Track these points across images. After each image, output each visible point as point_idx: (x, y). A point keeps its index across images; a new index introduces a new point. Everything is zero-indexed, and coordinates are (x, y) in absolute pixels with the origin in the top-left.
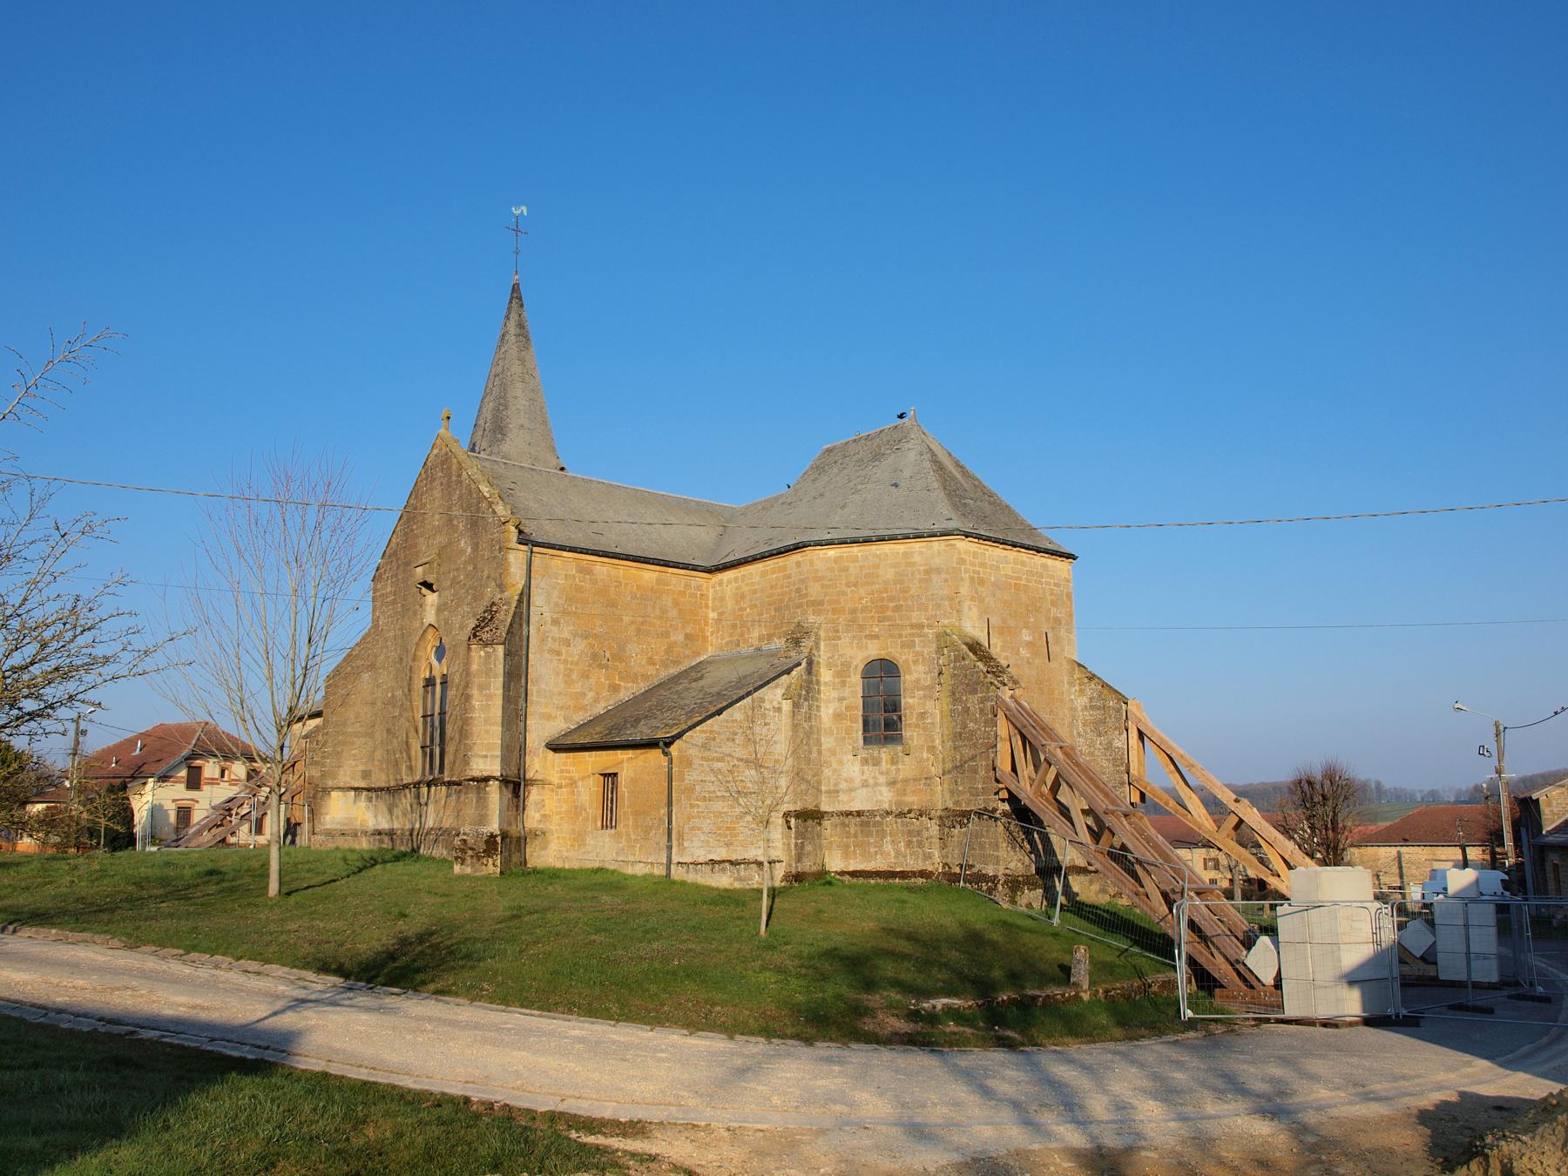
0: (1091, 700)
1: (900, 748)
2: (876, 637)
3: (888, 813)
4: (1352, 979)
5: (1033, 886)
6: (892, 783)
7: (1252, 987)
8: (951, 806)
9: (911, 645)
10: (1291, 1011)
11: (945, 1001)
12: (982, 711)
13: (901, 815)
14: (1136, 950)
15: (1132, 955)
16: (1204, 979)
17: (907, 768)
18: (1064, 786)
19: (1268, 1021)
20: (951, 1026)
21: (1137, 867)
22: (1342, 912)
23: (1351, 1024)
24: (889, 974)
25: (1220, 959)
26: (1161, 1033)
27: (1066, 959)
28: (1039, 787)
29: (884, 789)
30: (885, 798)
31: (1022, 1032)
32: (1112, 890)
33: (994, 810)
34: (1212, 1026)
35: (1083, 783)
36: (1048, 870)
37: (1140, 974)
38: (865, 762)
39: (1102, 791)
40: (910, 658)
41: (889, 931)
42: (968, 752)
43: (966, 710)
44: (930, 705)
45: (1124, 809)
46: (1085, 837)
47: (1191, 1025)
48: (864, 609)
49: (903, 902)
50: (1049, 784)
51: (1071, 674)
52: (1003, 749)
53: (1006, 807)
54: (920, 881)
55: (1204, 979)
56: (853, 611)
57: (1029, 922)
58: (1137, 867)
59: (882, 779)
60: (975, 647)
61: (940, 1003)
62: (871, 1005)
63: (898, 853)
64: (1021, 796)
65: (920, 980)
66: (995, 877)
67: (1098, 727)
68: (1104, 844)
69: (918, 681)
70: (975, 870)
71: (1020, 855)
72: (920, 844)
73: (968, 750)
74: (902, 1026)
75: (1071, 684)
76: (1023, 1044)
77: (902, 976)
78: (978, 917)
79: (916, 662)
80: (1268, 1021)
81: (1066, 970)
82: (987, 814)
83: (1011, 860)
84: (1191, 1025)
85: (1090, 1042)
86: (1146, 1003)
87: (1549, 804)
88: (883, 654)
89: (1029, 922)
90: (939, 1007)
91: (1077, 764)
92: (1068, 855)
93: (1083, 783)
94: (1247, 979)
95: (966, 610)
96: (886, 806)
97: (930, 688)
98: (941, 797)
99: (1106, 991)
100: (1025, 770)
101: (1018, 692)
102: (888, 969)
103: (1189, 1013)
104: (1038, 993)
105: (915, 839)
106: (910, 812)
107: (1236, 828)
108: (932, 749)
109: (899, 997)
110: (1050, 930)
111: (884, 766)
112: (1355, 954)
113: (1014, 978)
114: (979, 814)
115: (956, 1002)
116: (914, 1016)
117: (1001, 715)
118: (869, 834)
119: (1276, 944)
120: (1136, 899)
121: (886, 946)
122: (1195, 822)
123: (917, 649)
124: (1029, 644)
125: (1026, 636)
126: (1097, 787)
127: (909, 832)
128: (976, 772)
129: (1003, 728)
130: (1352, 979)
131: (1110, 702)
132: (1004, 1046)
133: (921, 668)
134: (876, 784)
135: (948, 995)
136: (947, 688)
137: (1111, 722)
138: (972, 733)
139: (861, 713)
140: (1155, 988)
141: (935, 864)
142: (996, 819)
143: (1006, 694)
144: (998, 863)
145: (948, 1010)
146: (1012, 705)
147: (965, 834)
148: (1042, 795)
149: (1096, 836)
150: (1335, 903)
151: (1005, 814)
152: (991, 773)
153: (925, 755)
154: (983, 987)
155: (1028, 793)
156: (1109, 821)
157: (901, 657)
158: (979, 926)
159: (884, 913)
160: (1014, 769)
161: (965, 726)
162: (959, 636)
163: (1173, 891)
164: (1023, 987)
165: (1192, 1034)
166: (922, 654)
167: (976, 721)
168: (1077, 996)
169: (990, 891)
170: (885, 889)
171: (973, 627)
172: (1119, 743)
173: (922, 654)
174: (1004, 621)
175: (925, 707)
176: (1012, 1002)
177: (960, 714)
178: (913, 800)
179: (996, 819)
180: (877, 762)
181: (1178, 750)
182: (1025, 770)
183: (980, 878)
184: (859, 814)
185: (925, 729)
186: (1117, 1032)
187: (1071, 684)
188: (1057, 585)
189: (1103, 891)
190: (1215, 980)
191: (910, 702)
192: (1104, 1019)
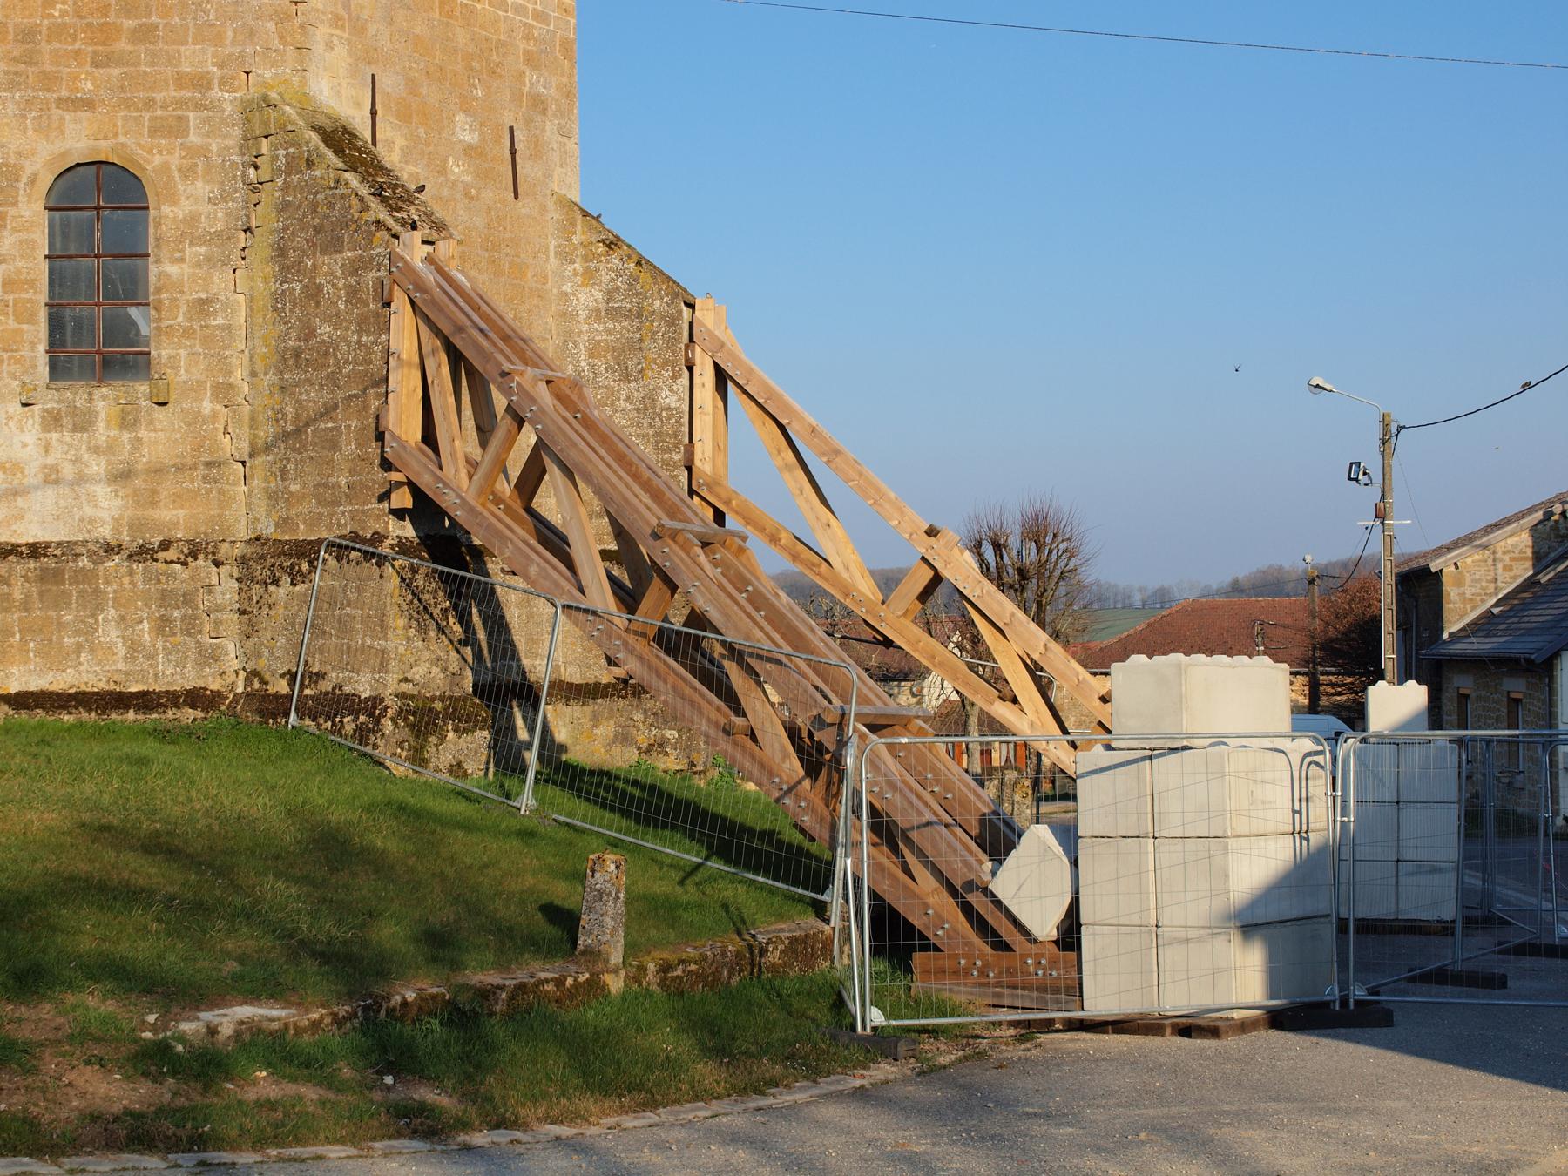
0: (610, 295)
1: (143, 388)
2: (87, 104)
3: (110, 549)
4: (1250, 923)
5: (466, 724)
6: (122, 476)
7: (999, 945)
8: (268, 530)
9: (177, 128)
10: (1099, 1000)
11: (245, 1011)
12: (353, 293)
13: (144, 553)
14: (715, 864)
15: (714, 878)
16: (895, 936)
17: (161, 437)
18: (554, 474)
19: (1047, 1026)
20: (262, 1084)
21: (731, 667)
22: (1236, 760)
23: (1244, 1027)
24: (86, 944)
25: (926, 882)
26: (814, 1073)
27: (561, 892)
28: (490, 478)
29: (102, 491)
30: (104, 511)
31: (470, 1090)
32: (643, 737)
33: (378, 538)
34: (928, 1045)
35: (601, 465)
36: (504, 691)
37: (740, 925)
38: (52, 420)
39: (647, 486)
40: (175, 161)
41: (102, 832)
42: (314, 398)
43: (314, 293)
44: (220, 282)
45: (698, 527)
46: (601, 597)
47: (883, 1044)
48: (58, 31)
49: (142, 761)
50: (515, 474)
51: (566, 231)
52: (404, 387)
53: (408, 530)
54: (189, 715)
55: (895, 936)
56: (28, 35)
57: (460, 808)
58: (731, 667)
59: (97, 466)
60: (338, 138)
61: (230, 1018)
62: (25, 1033)
63: (134, 647)
64: (447, 501)
65: (174, 958)
66: (376, 700)
67: (624, 361)
68: (649, 613)
69: (192, 220)
70: (326, 686)
71: (439, 647)
72: (191, 626)
73: (316, 380)
74: (115, 1092)
75: (565, 257)
76: (465, 1126)
77: (124, 949)
78: (334, 796)
79: (188, 173)
80: (1047, 1026)
81: (565, 921)
82: (360, 548)
83: (413, 658)
84: (883, 1044)
85: (651, 1104)
86: (758, 994)
87: (1459, 582)
88: (103, 150)
89: (460, 808)
90: (227, 1030)
91: (588, 423)
92: (551, 645)
93: (601, 465)
94: (992, 926)
95: (319, 48)
96: (106, 532)
97: (224, 238)
98: (244, 511)
99: (665, 968)
100: (458, 436)
101: (444, 249)
102: (87, 931)
103: (876, 1017)
104: (491, 978)
105: (177, 615)
106: (165, 545)
107: (925, 595)
108: (224, 392)
109: (111, 1006)
110: (515, 824)
111: (103, 431)
112: (1258, 864)
113: (439, 944)
114: (339, 549)
115: (272, 1013)
116: (155, 1059)
117: (400, 302)
118: (61, 602)
119: (1069, 836)
120: (725, 744)
121: (82, 867)
122: (837, 581)
123: (194, 138)
124: (469, 151)
125: (465, 132)
126: (636, 477)
127: (164, 596)
128: (334, 446)
129: (404, 333)
130: (1250, 923)
131: (657, 309)
132: (414, 1134)
133: (201, 188)
134: (81, 479)
135: (253, 997)
136: (263, 245)
137: (654, 348)
138: (327, 349)
139: (43, 297)
140: (773, 957)
141: (226, 674)
142: (382, 560)
143: (414, 250)
144: (383, 667)
145: (253, 1041)
146: (430, 276)
147: (305, 599)
148: (498, 500)
149: (629, 599)
150: (1219, 739)
151: (403, 547)
152: (373, 449)
153: (207, 406)
154: (354, 969)
155: (459, 484)
156: (669, 556)
157: (152, 158)
158: (337, 815)
159: (89, 789)
160: (429, 437)
161: (309, 333)
162: (302, 111)
163: (819, 721)
164: (456, 966)
165: (884, 1070)
166: (204, 152)
167: (336, 320)
168: (595, 987)
169: (362, 734)
170: (98, 733)
171: (336, 93)
172: (672, 397)
173: (204, 152)
174: (412, 87)
175: (207, 285)
176: (427, 1006)
177: (296, 298)
178: (175, 517)
179: (382, 560)
180: (83, 424)
181: (804, 412)
182: (458, 436)
183: (338, 704)
184: (36, 551)
185: (207, 341)
186: (708, 1072)
187: (565, 257)
188: (540, 16)
189: (624, 738)
190: (910, 929)
191: (172, 269)
192: (668, 1041)
